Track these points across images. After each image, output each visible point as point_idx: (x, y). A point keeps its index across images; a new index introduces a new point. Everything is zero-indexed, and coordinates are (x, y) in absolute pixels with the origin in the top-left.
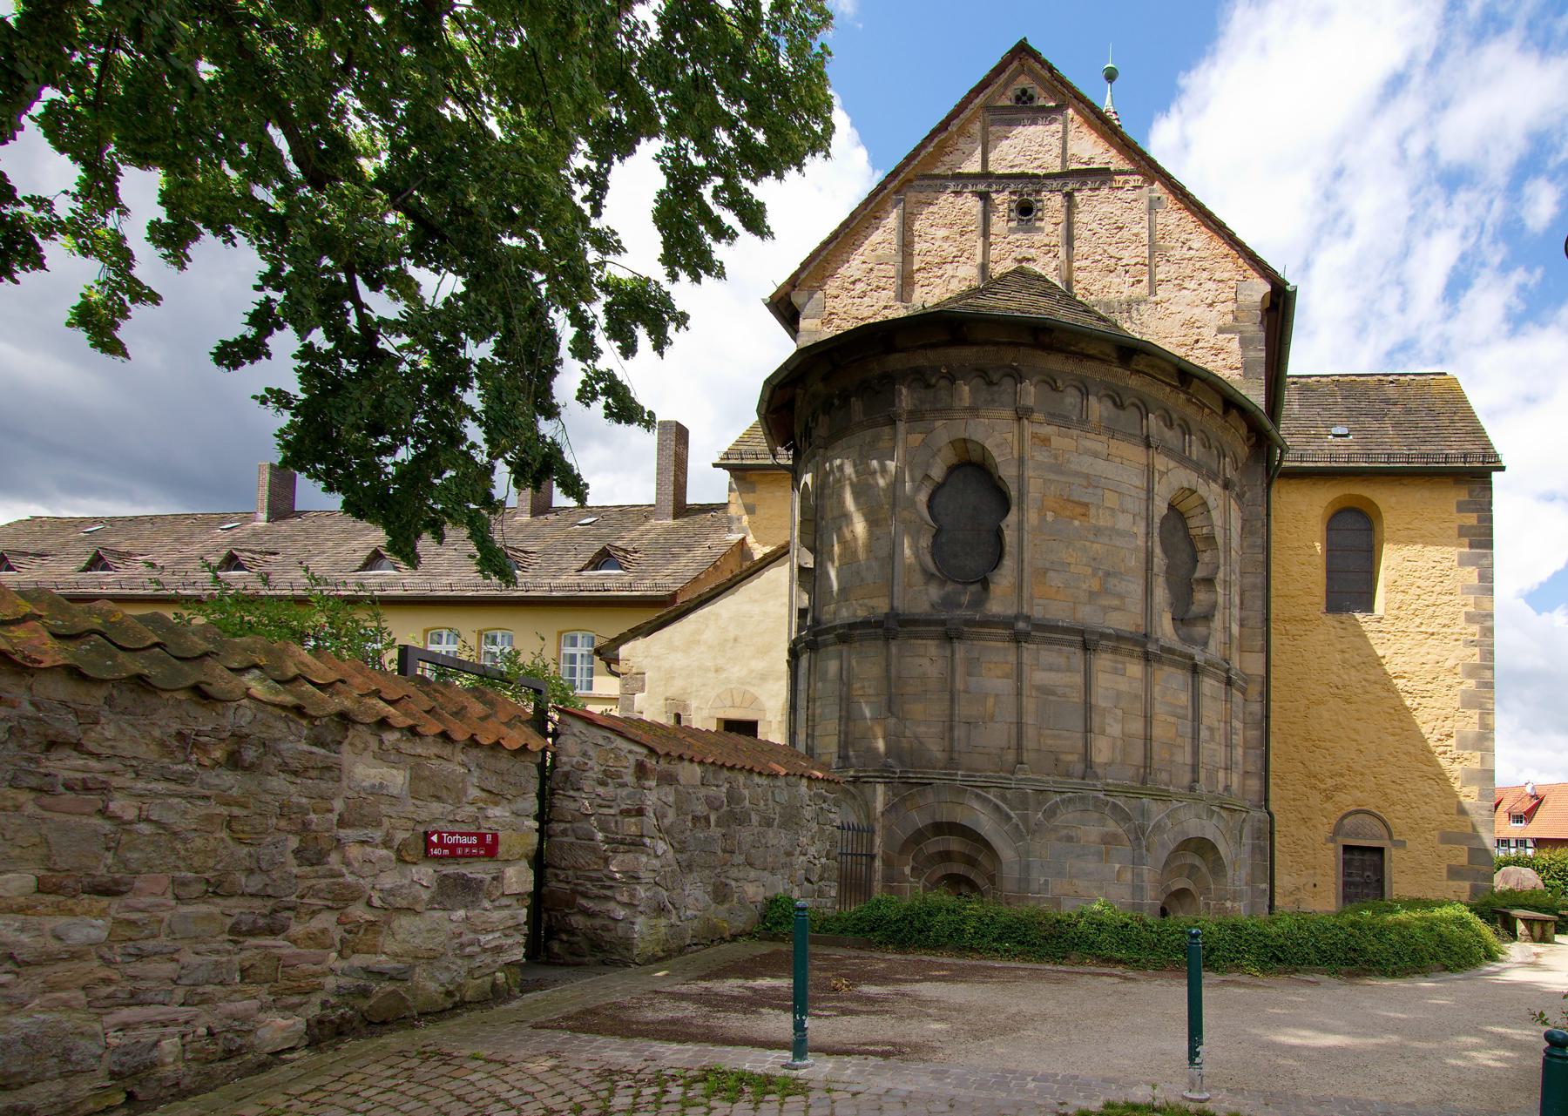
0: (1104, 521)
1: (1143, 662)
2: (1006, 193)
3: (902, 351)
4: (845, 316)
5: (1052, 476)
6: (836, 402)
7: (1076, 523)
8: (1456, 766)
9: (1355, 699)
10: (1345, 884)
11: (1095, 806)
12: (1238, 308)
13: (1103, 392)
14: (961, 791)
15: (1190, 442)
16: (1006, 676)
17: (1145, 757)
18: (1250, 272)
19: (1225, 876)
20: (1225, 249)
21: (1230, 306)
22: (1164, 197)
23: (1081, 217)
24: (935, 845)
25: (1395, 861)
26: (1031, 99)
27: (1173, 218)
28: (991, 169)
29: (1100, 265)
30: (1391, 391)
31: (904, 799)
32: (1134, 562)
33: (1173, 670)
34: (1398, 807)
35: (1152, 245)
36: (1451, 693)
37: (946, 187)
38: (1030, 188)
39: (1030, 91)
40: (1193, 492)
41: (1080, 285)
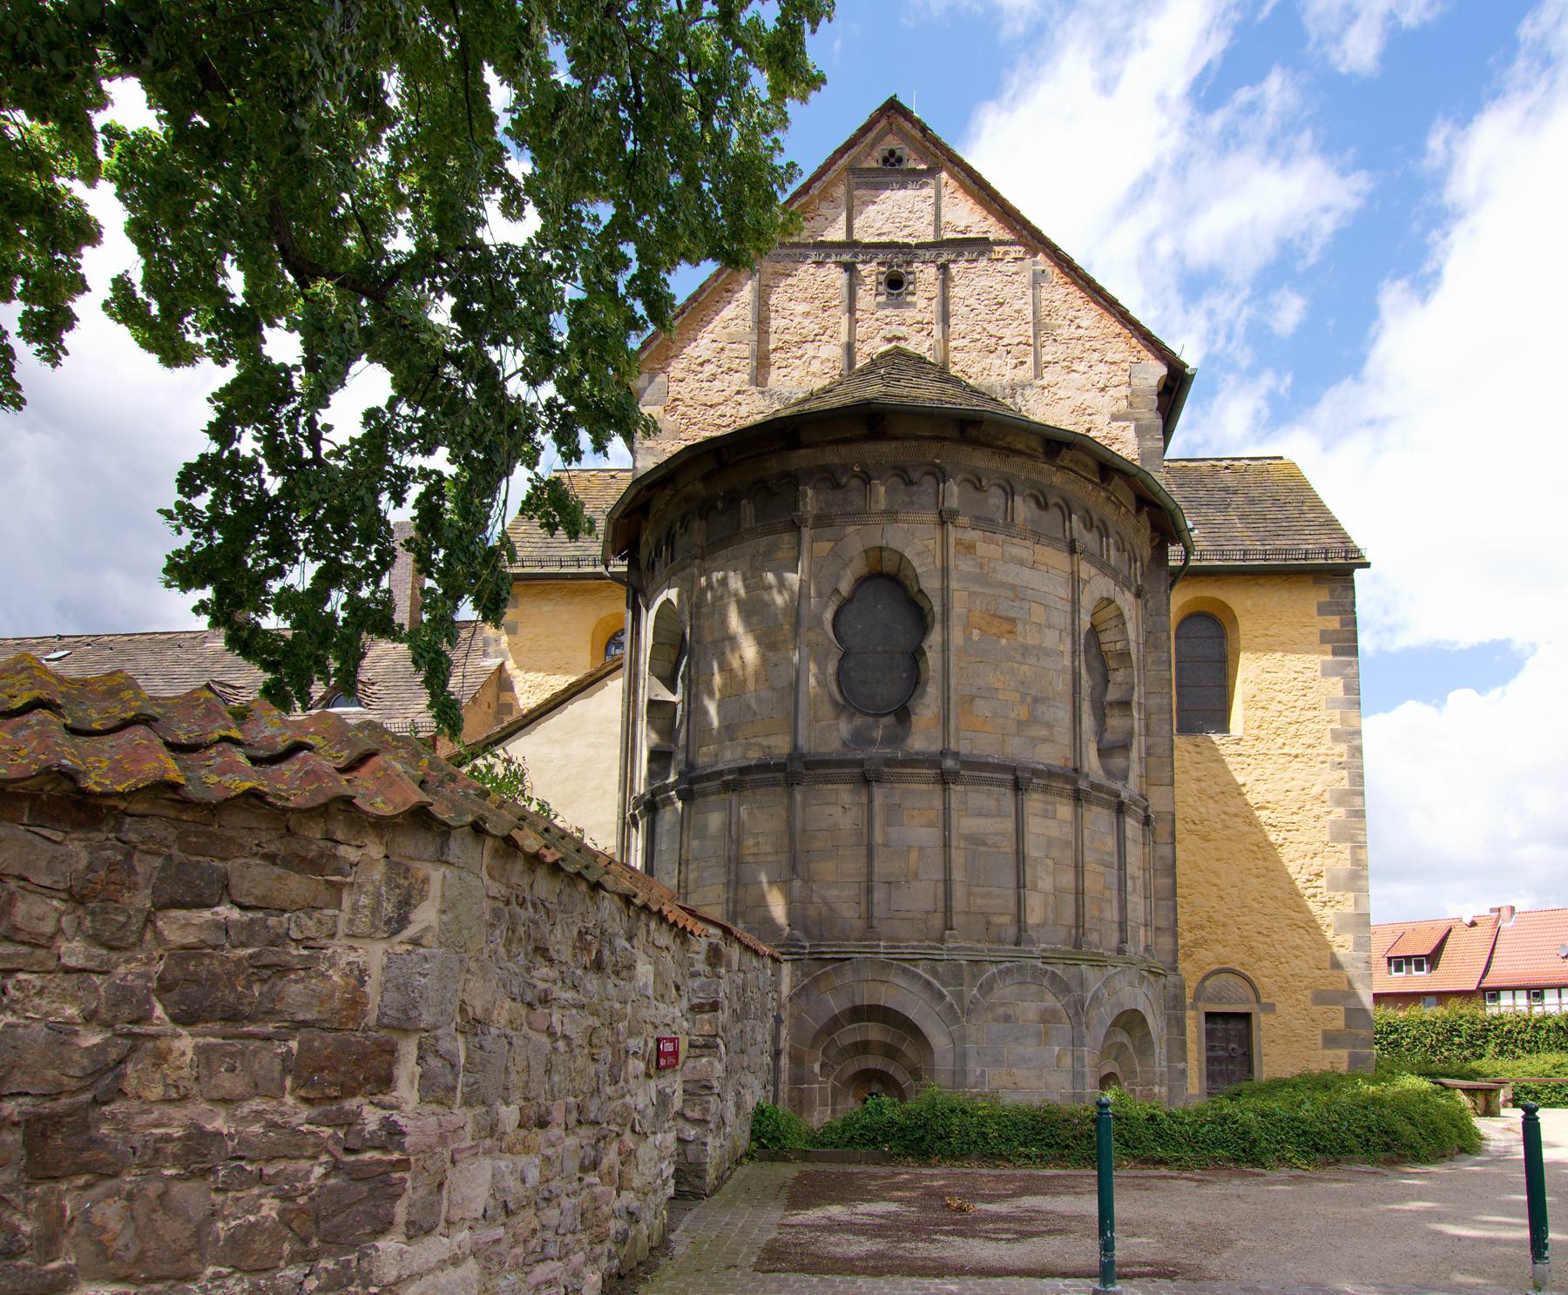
0: (1031, 639)
1: (1072, 802)
2: (874, 264)
3: (809, 446)
4: (691, 403)
5: (977, 589)
6: (720, 505)
7: (1004, 641)
8: (1328, 911)
9: (1213, 835)
10: (1210, 1060)
11: (1034, 977)
12: (1132, 394)
13: (1028, 491)
14: (885, 966)
15: (1108, 546)
16: (931, 825)
17: (1077, 916)
18: (1145, 353)
19: (1153, 1055)
20: (1117, 328)
21: (1124, 391)
22: (1049, 270)
23: (957, 291)
24: (850, 1034)
25: (1266, 1029)
26: (900, 160)
27: (1059, 293)
28: (857, 236)
29: (979, 345)
30: (1228, 479)
31: (816, 979)
32: (1062, 685)
33: (1100, 809)
34: (1266, 963)
35: (1038, 324)
36: (1319, 825)
37: (807, 257)
38: (900, 259)
39: (898, 153)
40: (1110, 601)
41: (957, 368)
